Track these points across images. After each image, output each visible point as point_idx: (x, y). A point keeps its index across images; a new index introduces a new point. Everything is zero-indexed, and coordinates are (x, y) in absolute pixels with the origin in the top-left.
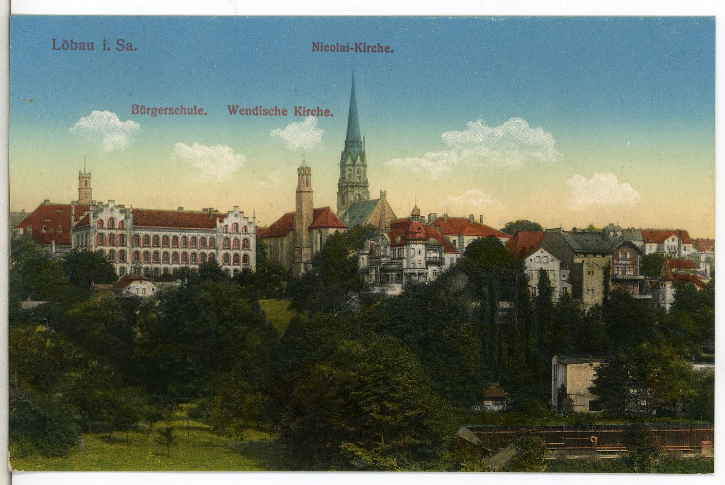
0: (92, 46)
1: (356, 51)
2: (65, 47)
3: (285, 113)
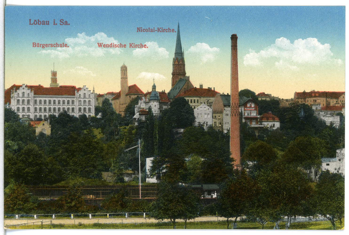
0: (48, 23)
1: (158, 32)
3: (125, 46)
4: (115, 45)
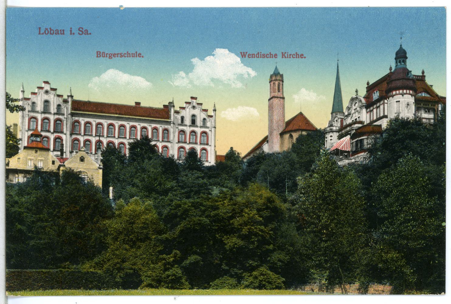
0: (63, 32)
2: (47, 32)
4: (263, 55)
